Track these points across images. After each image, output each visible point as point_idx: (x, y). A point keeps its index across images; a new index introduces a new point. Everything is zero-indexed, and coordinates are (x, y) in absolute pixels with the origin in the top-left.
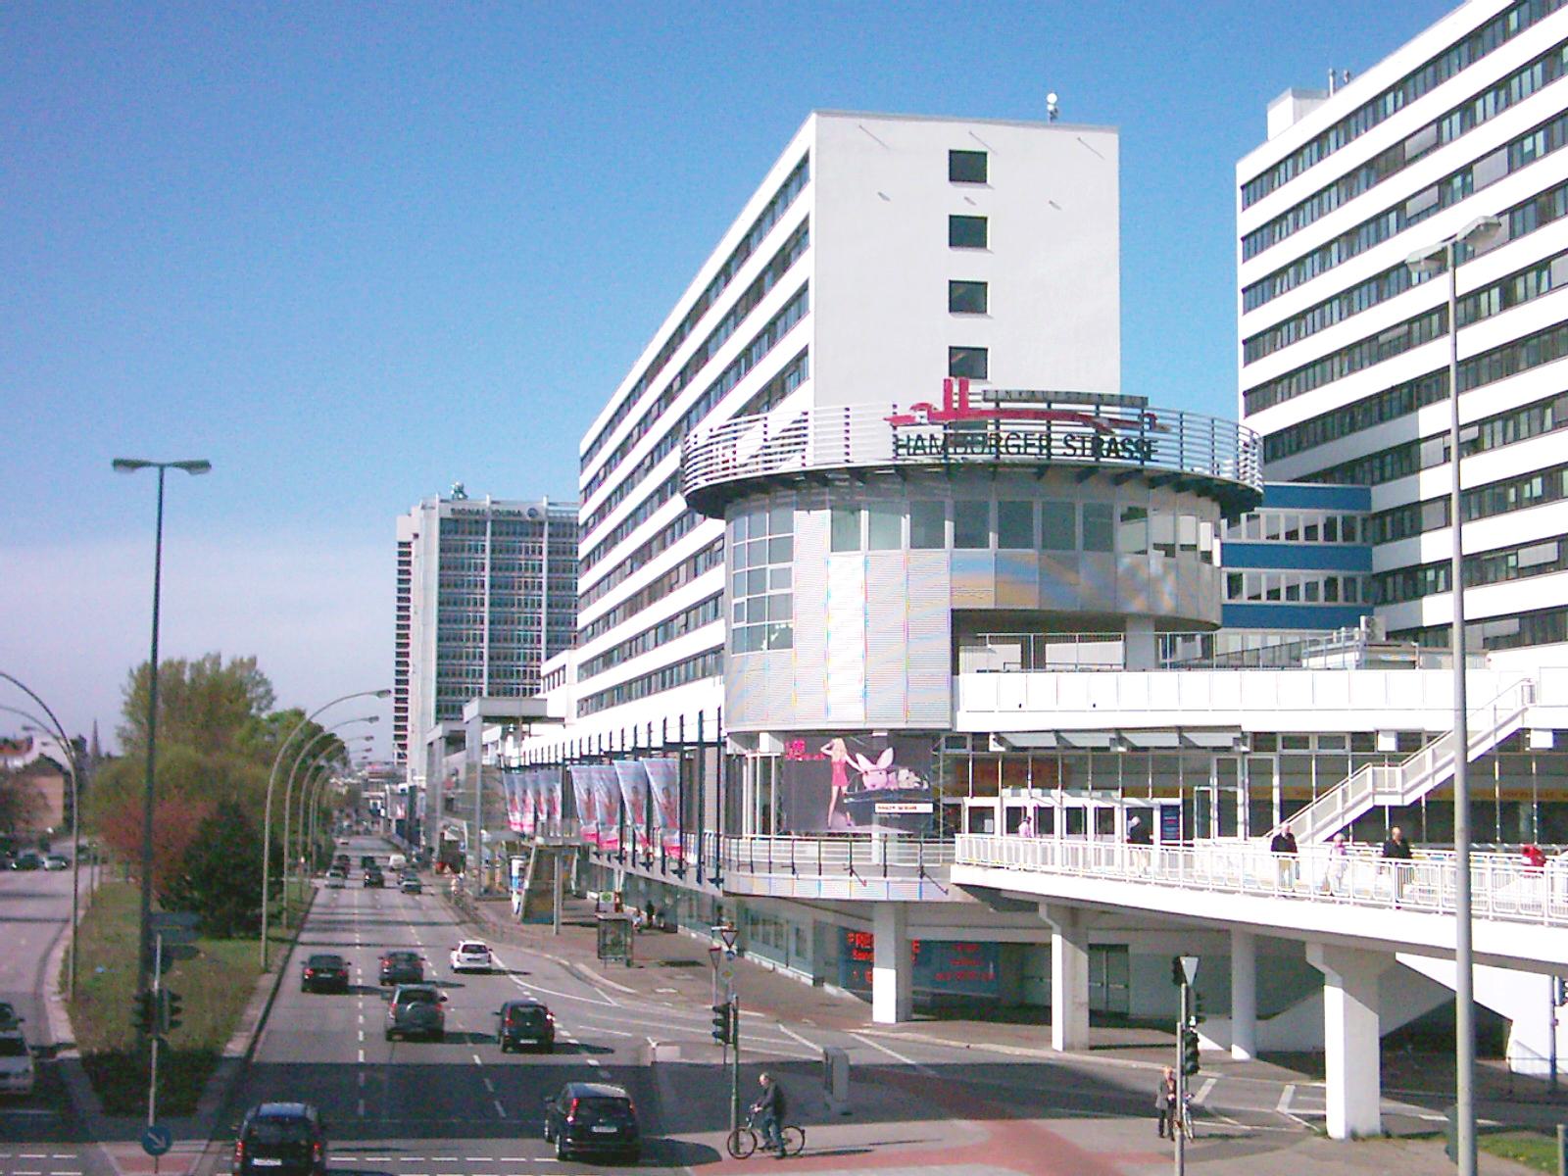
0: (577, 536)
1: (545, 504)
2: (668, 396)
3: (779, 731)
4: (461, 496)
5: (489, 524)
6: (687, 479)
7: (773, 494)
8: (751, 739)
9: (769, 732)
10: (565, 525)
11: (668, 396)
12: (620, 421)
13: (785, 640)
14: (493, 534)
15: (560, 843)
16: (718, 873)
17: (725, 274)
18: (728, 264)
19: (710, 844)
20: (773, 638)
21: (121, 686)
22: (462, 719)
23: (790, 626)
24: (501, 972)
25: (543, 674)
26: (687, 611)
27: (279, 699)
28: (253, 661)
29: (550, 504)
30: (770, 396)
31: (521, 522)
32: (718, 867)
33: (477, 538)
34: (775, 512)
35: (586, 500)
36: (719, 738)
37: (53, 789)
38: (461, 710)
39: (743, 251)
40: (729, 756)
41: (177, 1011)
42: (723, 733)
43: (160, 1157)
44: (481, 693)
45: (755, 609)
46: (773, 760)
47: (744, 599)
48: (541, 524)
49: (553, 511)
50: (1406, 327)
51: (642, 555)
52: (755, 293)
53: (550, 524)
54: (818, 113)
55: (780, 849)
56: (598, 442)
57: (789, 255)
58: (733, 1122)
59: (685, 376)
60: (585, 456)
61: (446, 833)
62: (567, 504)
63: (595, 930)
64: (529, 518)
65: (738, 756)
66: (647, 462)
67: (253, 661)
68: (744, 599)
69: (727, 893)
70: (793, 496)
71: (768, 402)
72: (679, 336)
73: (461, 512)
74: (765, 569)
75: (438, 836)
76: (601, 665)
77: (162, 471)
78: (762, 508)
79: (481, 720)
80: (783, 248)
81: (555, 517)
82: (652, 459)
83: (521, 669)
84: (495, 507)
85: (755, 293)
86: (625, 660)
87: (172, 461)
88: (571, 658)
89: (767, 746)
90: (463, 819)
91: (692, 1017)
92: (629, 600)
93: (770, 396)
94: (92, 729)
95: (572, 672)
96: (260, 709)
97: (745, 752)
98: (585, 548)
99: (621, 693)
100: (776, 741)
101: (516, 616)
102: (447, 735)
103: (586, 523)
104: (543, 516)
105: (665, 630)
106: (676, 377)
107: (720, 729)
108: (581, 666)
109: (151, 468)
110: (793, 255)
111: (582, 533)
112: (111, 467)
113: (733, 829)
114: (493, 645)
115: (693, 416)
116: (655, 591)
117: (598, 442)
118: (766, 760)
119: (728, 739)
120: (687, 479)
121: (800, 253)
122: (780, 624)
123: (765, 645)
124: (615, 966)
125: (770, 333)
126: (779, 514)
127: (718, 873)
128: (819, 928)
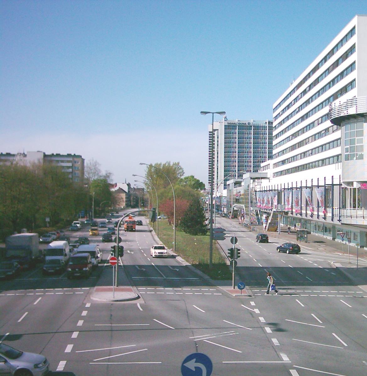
0: (272, 130)
1: (252, 121)
2: (305, 92)
3: (360, 181)
4: (226, 119)
5: (237, 126)
6: (332, 115)
7: (357, 119)
8: (351, 183)
9: (357, 182)
10: (257, 127)
11: (305, 92)
12: (287, 99)
13: (361, 157)
14: (238, 129)
15: (280, 211)
16: (340, 219)
17: (325, 59)
18: (326, 57)
19: (336, 211)
20: (357, 157)
21: (145, 170)
22: (243, 178)
23: (362, 154)
24: (271, 243)
25: (261, 166)
26: (312, 150)
27: (185, 173)
28: (179, 163)
29: (238, 121)
30: (341, 92)
31: (246, 126)
32: (340, 217)
33: (249, 131)
34: (357, 123)
35: (275, 120)
36: (340, 183)
37: (123, 196)
38: (242, 176)
39: (332, 53)
40: (343, 188)
41: (239, 253)
42: (341, 182)
43: (242, 290)
44: (251, 172)
45: (352, 149)
46: (357, 189)
47: (349, 147)
48: (251, 126)
49: (254, 123)
50: (332, 66)
51: (295, 135)
52: (336, 64)
53: (254, 126)
54: (358, 16)
55: (353, 212)
56: (280, 104)
57: (348, 54)
58: (233, 285)
59: (310, 87)
60: (275, 108)
61: (235, 208)
62: (260, 121)
63: (296, 233)
64: (248, 125)
65: (345, 188)
66: (297, 110)
67: (179, 163)
68: (349, 147)
69: (342, 224)
70: (363, 119)
71: (341, 94)
72: (309, 75)
73: (230, 123)
74: (355, 139)
75: (232, 209)
76: (281, 164)
77: (213, 114)
78: (355, 122)
79: (250, 178)
80: (346, 52)
81: (255, 125)
82: (299, 109)
83: (246, 165)
84: (239, 122)
85: (336, 64)
86: (290, 162)
87: (215, 112)
88: (272, 162)
89: (356, 185)
90: (243, 204)
91: (331, 255)
92: (292, 146)
93: (341, 92)
94: (125, 181)
95: (271, 166)
96: (180, 176)
97: (347, 187)
98: (275, 133)
99: (288, 171)
100: (358, 184)
101: (245, 151)
102: (235, 182)
103: (275, 126)
104: (251, 124)
105: (304, 154)
106: (308, 87)
107: (340, 181)
108: (274, 164)
109: (210, 113)
110: (349, 54)
111: (274, 129)
112: (200, 114)
113: (344, 207)
114: (239, 159)
115: (314, 97)
116: (300, 144)
117: (280, 104)
118: (354, 189)
119: (342, 183)
120: (332, 115)
121: (352, 54)
122: (359, 153)
123: (355, 158)
124: (302, 242)
125: (342, 75)
126: (359, 124)
127: (340, 219)
128: (361, 233)
